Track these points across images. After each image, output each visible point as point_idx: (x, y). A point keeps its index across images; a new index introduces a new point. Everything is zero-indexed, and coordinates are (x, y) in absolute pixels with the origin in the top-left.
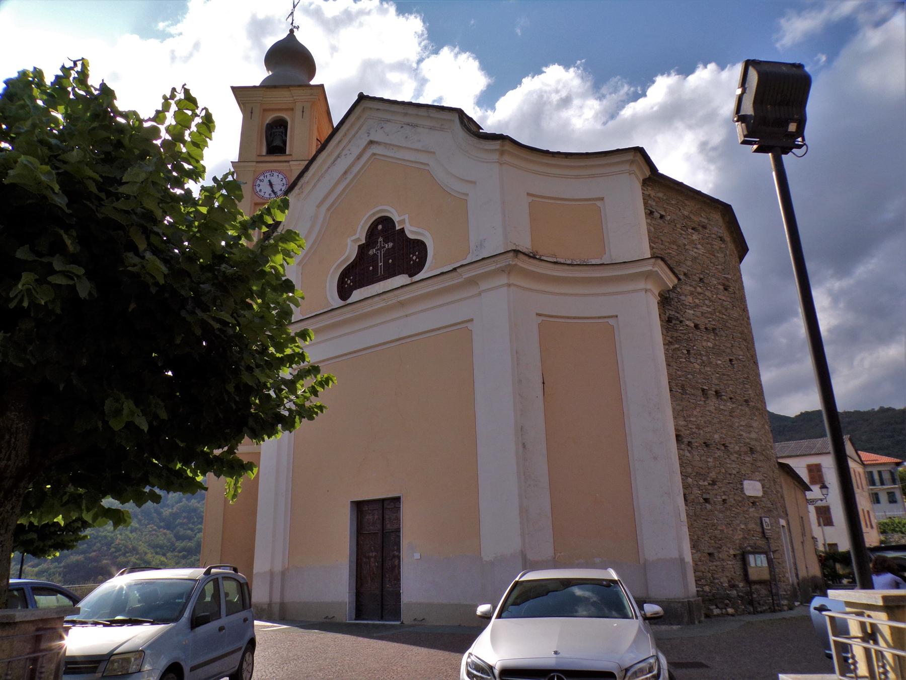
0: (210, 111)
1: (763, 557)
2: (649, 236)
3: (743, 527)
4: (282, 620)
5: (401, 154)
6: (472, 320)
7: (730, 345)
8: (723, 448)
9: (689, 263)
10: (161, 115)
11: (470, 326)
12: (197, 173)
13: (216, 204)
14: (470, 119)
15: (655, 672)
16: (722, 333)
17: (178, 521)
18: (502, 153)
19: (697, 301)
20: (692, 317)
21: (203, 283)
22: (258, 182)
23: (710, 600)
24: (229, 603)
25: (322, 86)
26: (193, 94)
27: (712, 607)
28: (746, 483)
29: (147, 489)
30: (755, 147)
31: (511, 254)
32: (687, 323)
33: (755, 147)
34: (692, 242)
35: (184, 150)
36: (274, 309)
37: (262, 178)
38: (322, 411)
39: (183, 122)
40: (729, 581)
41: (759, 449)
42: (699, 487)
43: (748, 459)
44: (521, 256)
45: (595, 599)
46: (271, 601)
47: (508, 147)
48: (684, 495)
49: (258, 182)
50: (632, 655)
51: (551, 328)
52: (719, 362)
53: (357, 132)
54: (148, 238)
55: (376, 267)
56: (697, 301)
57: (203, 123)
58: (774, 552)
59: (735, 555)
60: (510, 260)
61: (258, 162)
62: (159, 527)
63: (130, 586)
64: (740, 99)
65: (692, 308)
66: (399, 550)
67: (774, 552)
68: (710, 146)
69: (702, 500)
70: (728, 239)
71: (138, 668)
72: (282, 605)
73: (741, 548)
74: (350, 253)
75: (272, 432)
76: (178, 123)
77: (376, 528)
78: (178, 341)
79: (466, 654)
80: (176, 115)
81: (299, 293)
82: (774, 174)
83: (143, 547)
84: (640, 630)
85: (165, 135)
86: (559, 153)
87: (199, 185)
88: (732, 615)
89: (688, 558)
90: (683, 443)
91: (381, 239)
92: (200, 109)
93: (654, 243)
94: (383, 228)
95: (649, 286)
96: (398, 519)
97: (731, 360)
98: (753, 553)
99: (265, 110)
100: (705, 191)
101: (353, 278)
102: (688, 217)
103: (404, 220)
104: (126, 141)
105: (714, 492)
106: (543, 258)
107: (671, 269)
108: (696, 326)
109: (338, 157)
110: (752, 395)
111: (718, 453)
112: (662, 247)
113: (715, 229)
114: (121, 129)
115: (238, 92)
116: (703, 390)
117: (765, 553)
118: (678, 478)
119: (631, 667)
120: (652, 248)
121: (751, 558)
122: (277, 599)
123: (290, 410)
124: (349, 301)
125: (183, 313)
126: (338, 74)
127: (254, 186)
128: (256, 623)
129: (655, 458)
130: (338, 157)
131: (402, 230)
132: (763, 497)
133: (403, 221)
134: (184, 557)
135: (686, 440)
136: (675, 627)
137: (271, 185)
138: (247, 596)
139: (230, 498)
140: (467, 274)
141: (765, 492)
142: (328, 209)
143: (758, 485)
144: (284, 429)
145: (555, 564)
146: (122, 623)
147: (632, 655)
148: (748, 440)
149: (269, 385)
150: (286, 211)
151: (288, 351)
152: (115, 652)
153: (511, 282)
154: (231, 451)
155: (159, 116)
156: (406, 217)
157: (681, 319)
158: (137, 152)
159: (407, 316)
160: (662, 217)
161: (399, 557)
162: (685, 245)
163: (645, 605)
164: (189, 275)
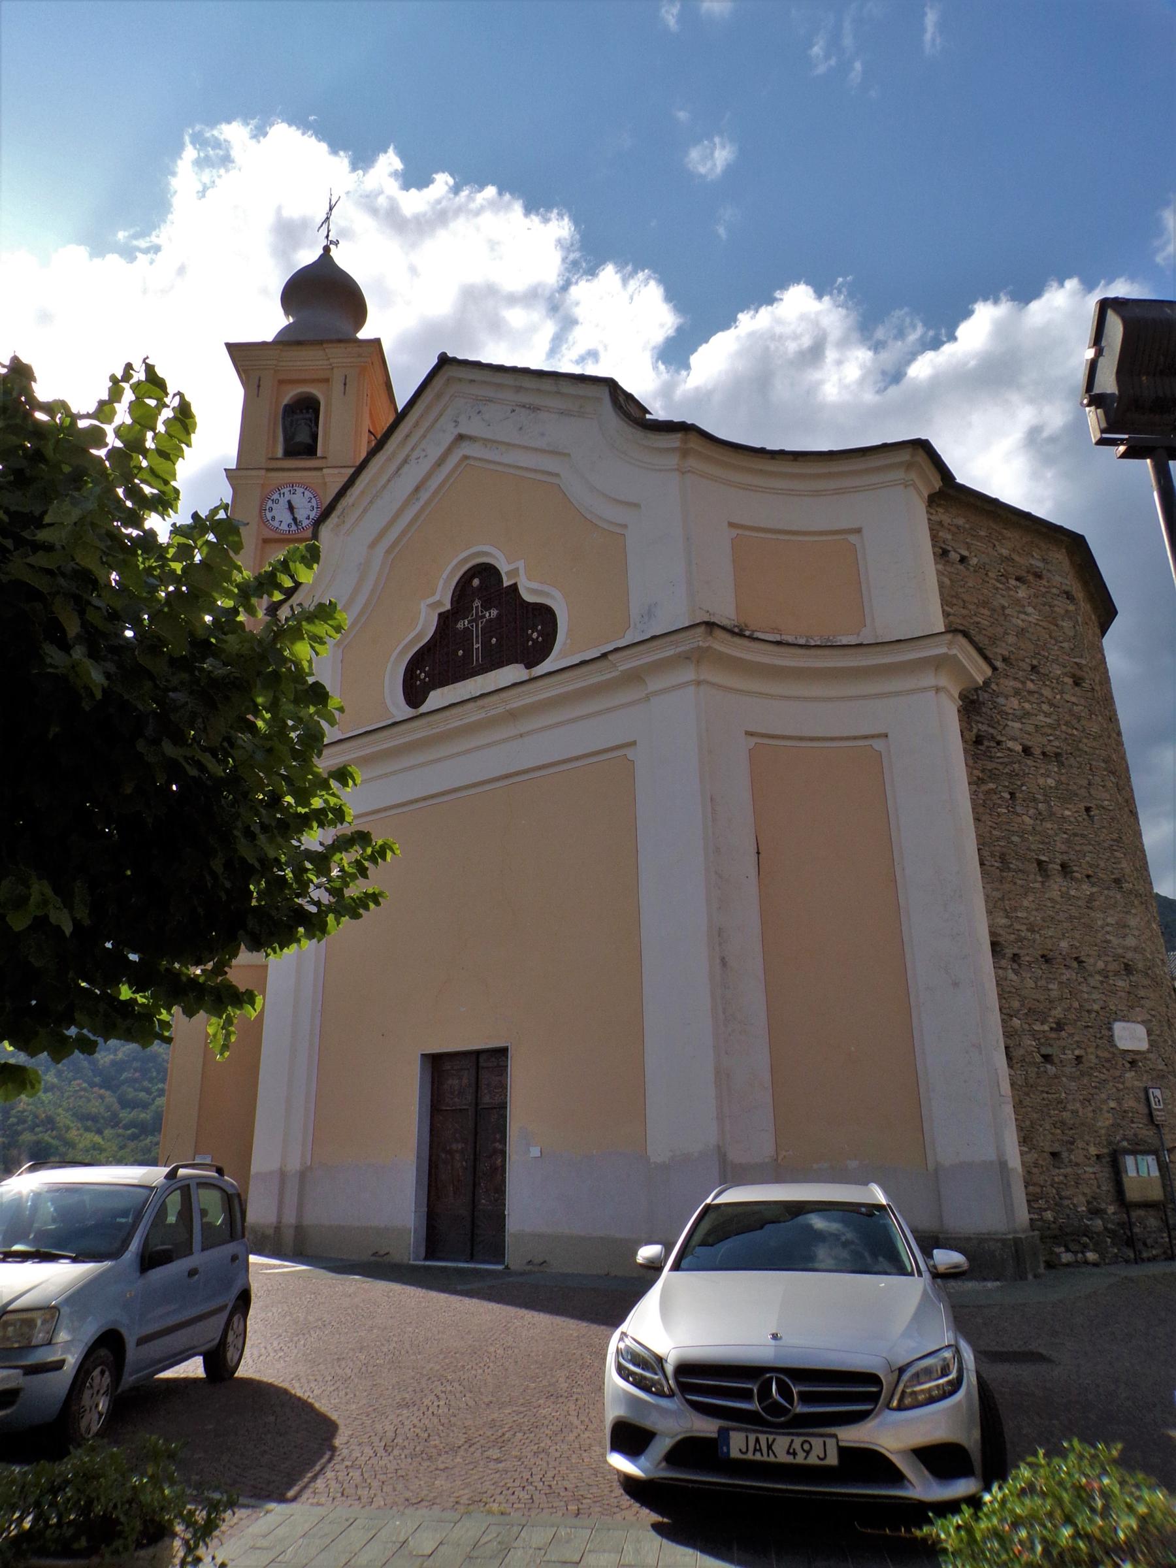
0: (187, 398)
1: (1151, 1159)
2: (941, 594)
3: (1112, 1104)
4: (298, 1254)
5: (510, 458)
6: (634, 743)
7: (1085, 783)
8: (1075, 964)
9: (1011, 639)
10: (106, 408)
11: (630, 753)
12: (164, 502)
13: (198, 558)
14: (630, 397)
15: (953, 1376)
16: (1072, 760)
17: (125, 1075)
18: (685, 453)
19: (1027, 706)
20: (1018, 733)
21: (175, 690)
22: (270, 503)
23: (1055, 1237)
24: (207, 1228)
25: (377, 342)
26: (160, 372)
27: (1057, 1250)
28: (1118, 1027)
29: (72, 1031)
30: (1122, 448)
31: (702, 629)
32: (1010, 744)
33: (1122, 448)
34: (1018, 602)
35: (144, 464)
36: (294, 729)
37: (276, 496)
38: (377, 903)
39: (144, 418)
40: (1088, 1202)
41: (1140, 966)
42: (1034, 1034)
43: (1120, 983)
44: (719, 633)
45: (849, 1235)
47: (694, 443)
48: (1007, 1048)
49: (270, 503)
50: (912, 1344)
51: (769, 754)
52: (1067, 813)
53: (436, 420)
54: (82, 613)
55: (468, 651)
56: (1027, 706)
57: (175, 418)
58: (1170, 1151)
59: (1098, 1156)
60: (698, 639)
61: (268, 470)
62: (92, 1085)
63: (37, 1196)
64: (1093, 366)
65: (1019, 719)
66: (503, 1140)
67: (1170, 1151)
68: (1045, 434)
69: (1039, 1059)
70: (1080, 595)
71: (48, 1336)
72: (299, 1229)
73: (1110, 1143)
74: (425, 626)
75: (286, 938)
76: (134, 421)
77: (465, 1100)
78: (128, 789)
79: (617, 1335)
80: (132, 407)
81: (334, 702)
82: (1156, 495)
83: (63, 1118)
84: (925, 1292)
85: (113, 441)
86: (782, 453)
87: (169, 521)
88: (1096, 1265)
89: (1015, 1161)
90: (1004, 957)
91: (477, 603)
92: (170, 396)
93: (952, 605)
94: (481, 584)
95: (943, 681)
96: (503, 1087)
97: (1088, 809)
98: (1134, 1153)
99: (281, 382)
100: (1040, 512)
101: (432, 667)
102: (1008, 559)
103: (517, 569)
104: (49, 451)
105: (1062, 1043)
106: (757, 635)
107: (981, 651)
108: (1027, 751)
109: (405, 461)
110: (1127, 871)
111: (1067, 974)
112: (965, 612)
113: (1058, 578)
114: (39, 431)
115: (237, 351)
116: (1040, 863)
117: (1155, 1152)
118: (995, 1018)
119: (909, 1364)
120: (946, 615)
121: (1129, 1161)
122: (290, 1218)
123: (318, 904)
124: (424, 708)
125: (141, 746)
126: (401, 321)
127: (262, 510)
128: (253, 1259)
129: (956, 984)
130: (405, 461)
131: (514, 588)
132: (1149, 1051)
133: (514, 572)
134: (134, 1137)
135: (1009, 952)
136: (990, 1285)
137: (291, 508)
138: (238, 1215)
139: (217, 1050)
140: (625, 663)
141: (1152, 1043)
142: (388, 552)
143: (1141, 1030)
144: (310, 935)
145: (778, 1176)
146: (23, 1257)
147: (912, 1344)
148: (1120, 951)
149: (283, 859)
150: (315, 566)
151: (317, 803)
152: (11, 1308)
153: (702, 678)
154: (219, 970)
155: (104, 410)
156: (520, 564)
157: (999, 738)
158: (67, 469)
159: (521, 736)
160: (963, 559)
161: (503, 1153)
162: (1003, 608)
163: (935, 1251)
164: (152, 677)
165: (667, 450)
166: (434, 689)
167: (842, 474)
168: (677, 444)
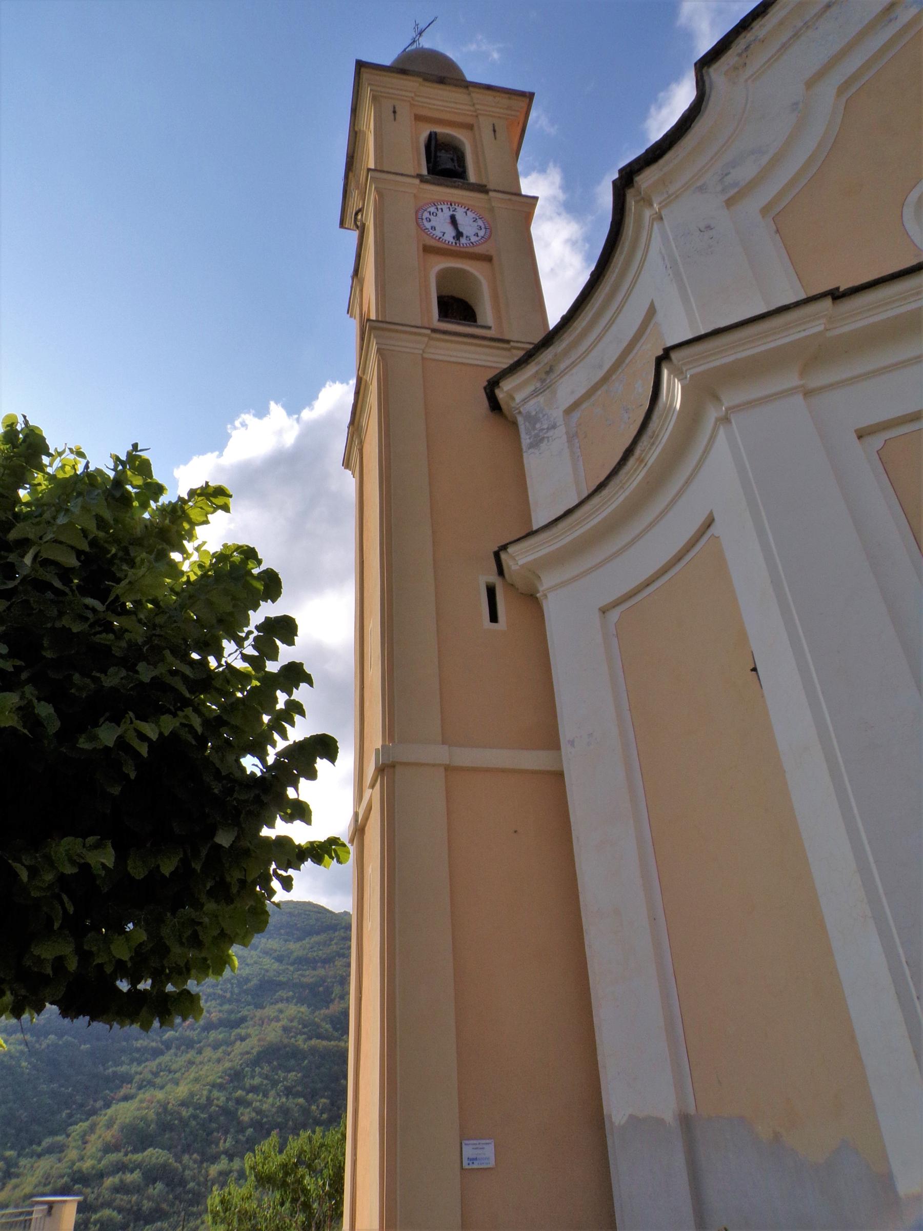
37: (432, 209)
127: (418, 220)
142: (842, 90)
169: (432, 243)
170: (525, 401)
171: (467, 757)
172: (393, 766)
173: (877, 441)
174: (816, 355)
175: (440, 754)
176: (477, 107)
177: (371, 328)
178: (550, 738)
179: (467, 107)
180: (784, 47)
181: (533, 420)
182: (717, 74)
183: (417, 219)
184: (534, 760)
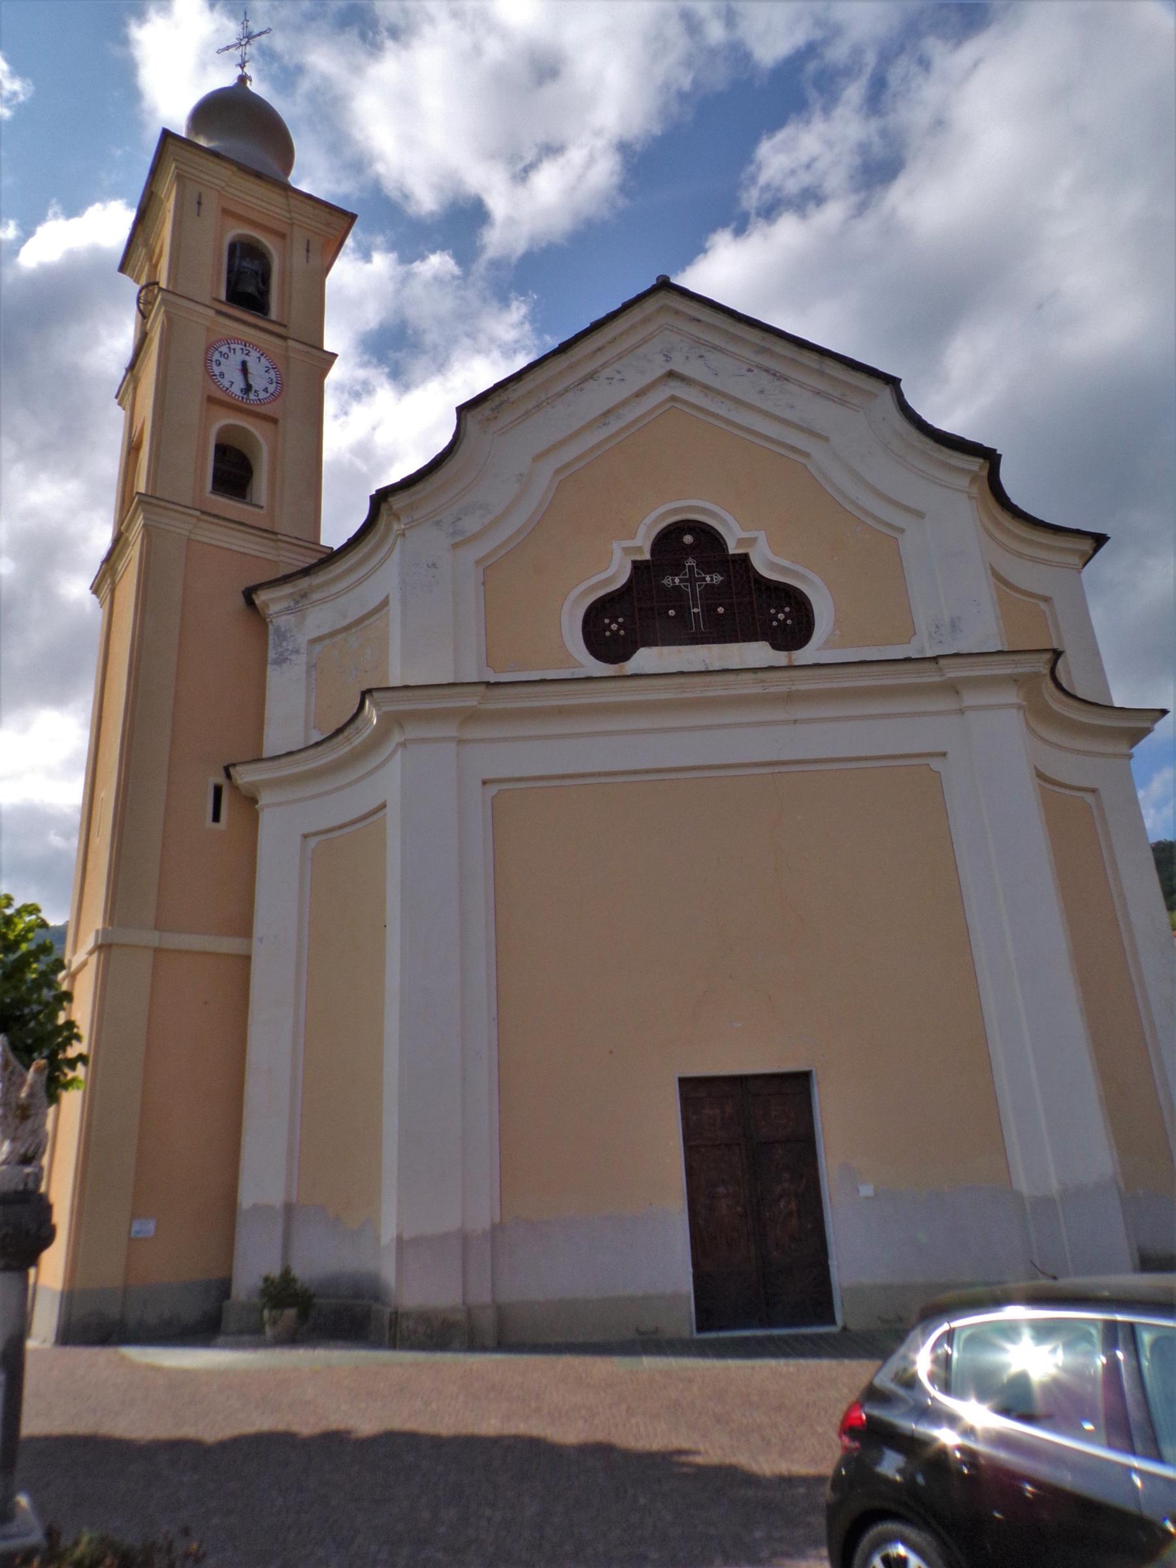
37: (224, 349)
46: (286, 1272)
49: (216, 356)
103: (754, 540)
127: (207, 360)
130: (591, 376)
131: (745, 558)
140: (954, 671)
142: (557, 472)
165: (962, 471)
166: (643, 646)
167: (1041, 545)
168: (976, 468)
169: (219, 395)
170: (279, 613)
171: (174, 941)
172: (110, 946)
173: (493, 790)
174: (471, 717)
175: (153, 938)
176: (295, 215)
177: (140, 502)
178: (244, 926)
179: (284, 213)
180: (528, 413)
181: (282, 636)
182: (471, 417)
183: (206, 359)
184: (229, 945)
